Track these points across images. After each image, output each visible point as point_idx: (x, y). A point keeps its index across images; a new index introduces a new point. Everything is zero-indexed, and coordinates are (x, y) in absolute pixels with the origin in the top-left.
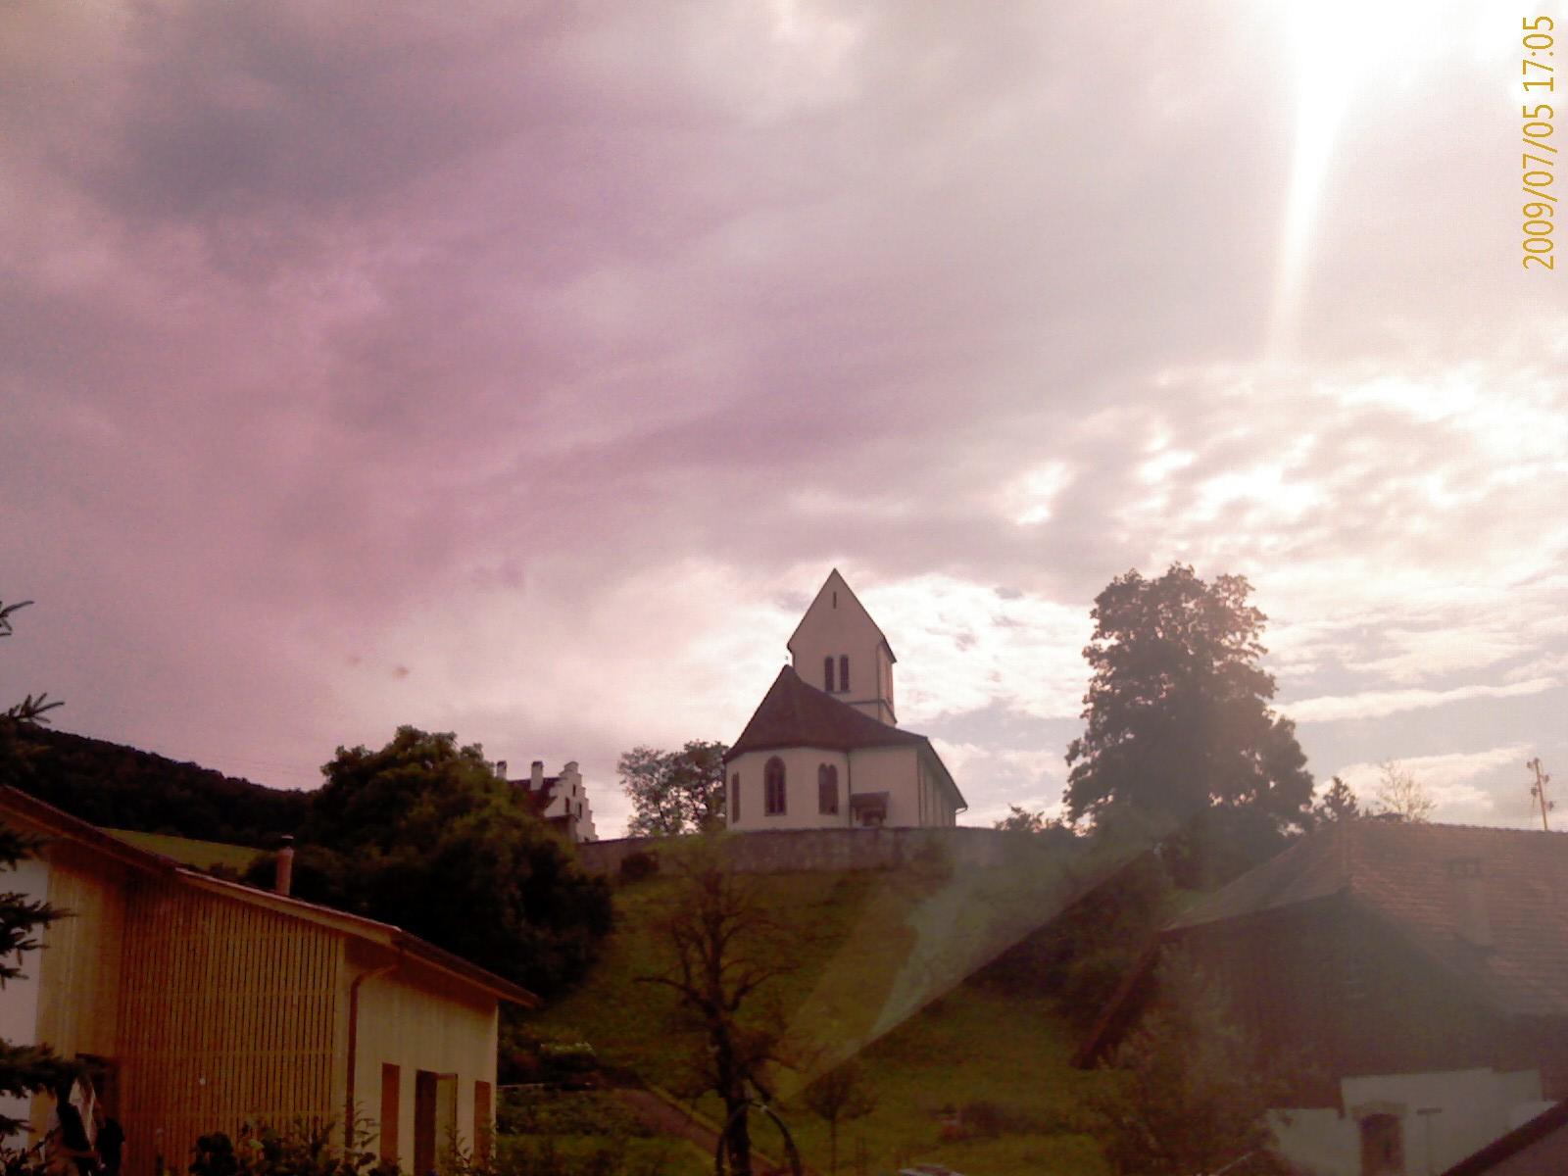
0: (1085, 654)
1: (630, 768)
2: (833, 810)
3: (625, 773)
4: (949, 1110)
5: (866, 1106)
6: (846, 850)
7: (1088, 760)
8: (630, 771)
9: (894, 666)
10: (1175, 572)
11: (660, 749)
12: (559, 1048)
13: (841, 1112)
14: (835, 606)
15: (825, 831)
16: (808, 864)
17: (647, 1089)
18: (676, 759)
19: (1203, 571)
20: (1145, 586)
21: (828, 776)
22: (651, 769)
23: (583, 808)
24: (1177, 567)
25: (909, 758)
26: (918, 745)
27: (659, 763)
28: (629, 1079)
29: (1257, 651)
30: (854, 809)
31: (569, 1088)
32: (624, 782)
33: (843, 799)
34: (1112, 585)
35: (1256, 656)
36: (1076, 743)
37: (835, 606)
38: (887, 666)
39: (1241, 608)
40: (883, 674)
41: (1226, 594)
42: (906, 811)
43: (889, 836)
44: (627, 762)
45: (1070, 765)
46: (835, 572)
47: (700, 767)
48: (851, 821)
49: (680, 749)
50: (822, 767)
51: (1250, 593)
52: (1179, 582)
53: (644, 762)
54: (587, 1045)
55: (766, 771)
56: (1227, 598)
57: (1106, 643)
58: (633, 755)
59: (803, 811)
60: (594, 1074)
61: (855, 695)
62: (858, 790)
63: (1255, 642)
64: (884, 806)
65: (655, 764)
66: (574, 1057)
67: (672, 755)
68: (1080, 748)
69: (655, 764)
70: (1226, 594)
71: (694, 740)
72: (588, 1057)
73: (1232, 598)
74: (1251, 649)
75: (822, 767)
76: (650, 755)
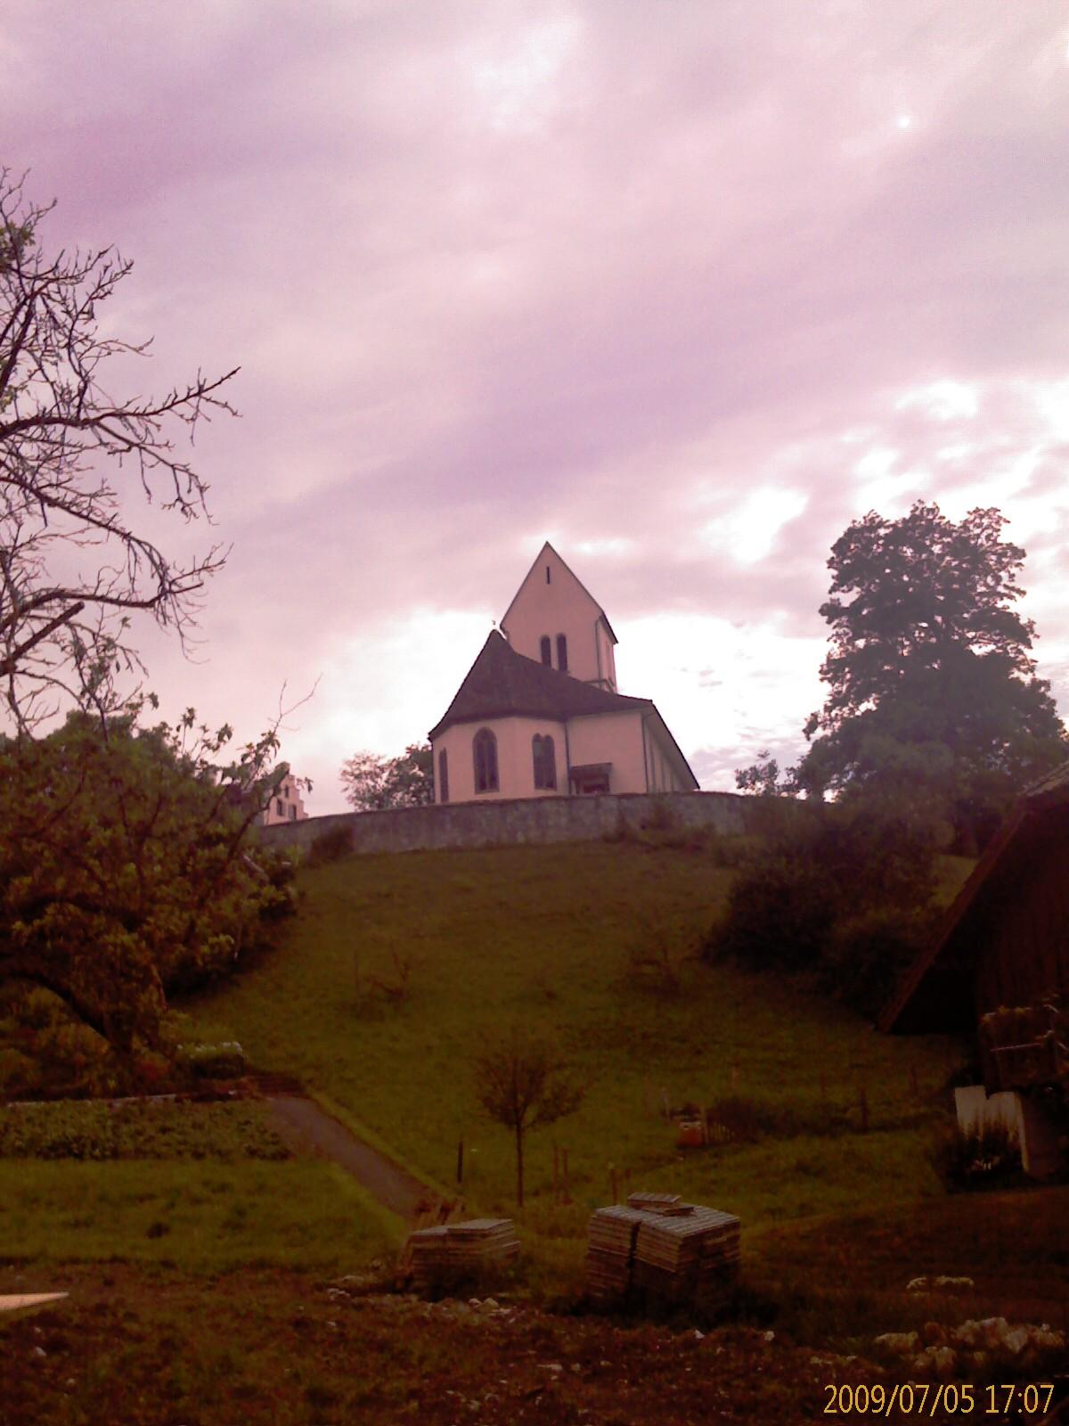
0: (822, 612)
1: (352, 774)
2: (551, 785)
3: (348, 780)
4: (689, 1112)
5: (567, 1105)
6: (564, 821)
7: (828, 732)
8: (352, 778)
9: (616, 646)
10: (918, 513)
11: (381, 755)
12: (201, 1050)
13: (530, 1114)
14: (549, 582)
15: (540, 800)
16: (521, 838)
17: (308, 1097)
18: (398, 764)
19: (954, 511)
20: (888, 527)
21: (544, 749)
22: (374, 775)
23: (298, 809)
24: (921, 506)
25: (631, 726)
26: (645, 710)
27: (382, 769)
28: (292, 1087)
29: (1014, 594)
30: (573, 783)
31: (205, 1098)
32: (346, 789)
33: (561, 771)
34: (850, 529)
35: (1011, 597)
36: (814, 716)
37: (549, 582)
38: (608, 647)
39: (995, 543)
40: (604, 657)
41: (977, 531)
42: (631, 775)
43: (612, 803)
44: (349, 769)
45: (809, 739)
46: (547, 545)
47: (423, 772)
48: (570, 792)
49: (402, 754)
50: (537, 738)
51: (1004, 526)
52: (921, 524)
53: (365, 768)
54: (237, 1044)
55: (474, 740)
56: (978, 536)
57: (847, 598)
58: (354, 761)
59: (517, 780)
60: (244, 1080)
61: (579, 669)
62: (577, 762)
63: (1011, 584)
64: (606, 777)
65: (378, 770)
66: (222, 1059)
67: (394, 760)
68: (819, 720)
69: (378, 770)
70: (977, 531)
71: (415, 743)
72: (239, 1059)
73: (985, 534)
74: (1007, 591)
75: (537, 738)
76: (371, 761)
